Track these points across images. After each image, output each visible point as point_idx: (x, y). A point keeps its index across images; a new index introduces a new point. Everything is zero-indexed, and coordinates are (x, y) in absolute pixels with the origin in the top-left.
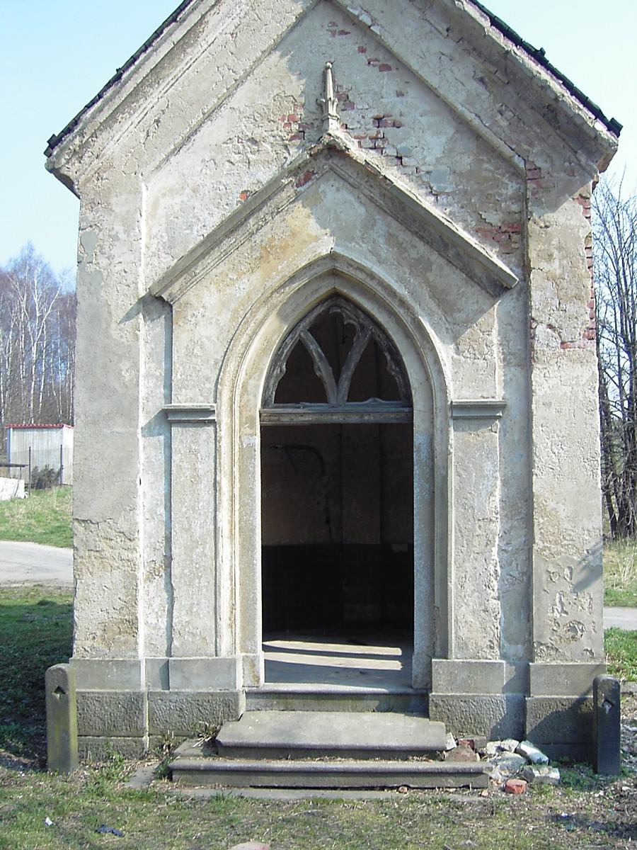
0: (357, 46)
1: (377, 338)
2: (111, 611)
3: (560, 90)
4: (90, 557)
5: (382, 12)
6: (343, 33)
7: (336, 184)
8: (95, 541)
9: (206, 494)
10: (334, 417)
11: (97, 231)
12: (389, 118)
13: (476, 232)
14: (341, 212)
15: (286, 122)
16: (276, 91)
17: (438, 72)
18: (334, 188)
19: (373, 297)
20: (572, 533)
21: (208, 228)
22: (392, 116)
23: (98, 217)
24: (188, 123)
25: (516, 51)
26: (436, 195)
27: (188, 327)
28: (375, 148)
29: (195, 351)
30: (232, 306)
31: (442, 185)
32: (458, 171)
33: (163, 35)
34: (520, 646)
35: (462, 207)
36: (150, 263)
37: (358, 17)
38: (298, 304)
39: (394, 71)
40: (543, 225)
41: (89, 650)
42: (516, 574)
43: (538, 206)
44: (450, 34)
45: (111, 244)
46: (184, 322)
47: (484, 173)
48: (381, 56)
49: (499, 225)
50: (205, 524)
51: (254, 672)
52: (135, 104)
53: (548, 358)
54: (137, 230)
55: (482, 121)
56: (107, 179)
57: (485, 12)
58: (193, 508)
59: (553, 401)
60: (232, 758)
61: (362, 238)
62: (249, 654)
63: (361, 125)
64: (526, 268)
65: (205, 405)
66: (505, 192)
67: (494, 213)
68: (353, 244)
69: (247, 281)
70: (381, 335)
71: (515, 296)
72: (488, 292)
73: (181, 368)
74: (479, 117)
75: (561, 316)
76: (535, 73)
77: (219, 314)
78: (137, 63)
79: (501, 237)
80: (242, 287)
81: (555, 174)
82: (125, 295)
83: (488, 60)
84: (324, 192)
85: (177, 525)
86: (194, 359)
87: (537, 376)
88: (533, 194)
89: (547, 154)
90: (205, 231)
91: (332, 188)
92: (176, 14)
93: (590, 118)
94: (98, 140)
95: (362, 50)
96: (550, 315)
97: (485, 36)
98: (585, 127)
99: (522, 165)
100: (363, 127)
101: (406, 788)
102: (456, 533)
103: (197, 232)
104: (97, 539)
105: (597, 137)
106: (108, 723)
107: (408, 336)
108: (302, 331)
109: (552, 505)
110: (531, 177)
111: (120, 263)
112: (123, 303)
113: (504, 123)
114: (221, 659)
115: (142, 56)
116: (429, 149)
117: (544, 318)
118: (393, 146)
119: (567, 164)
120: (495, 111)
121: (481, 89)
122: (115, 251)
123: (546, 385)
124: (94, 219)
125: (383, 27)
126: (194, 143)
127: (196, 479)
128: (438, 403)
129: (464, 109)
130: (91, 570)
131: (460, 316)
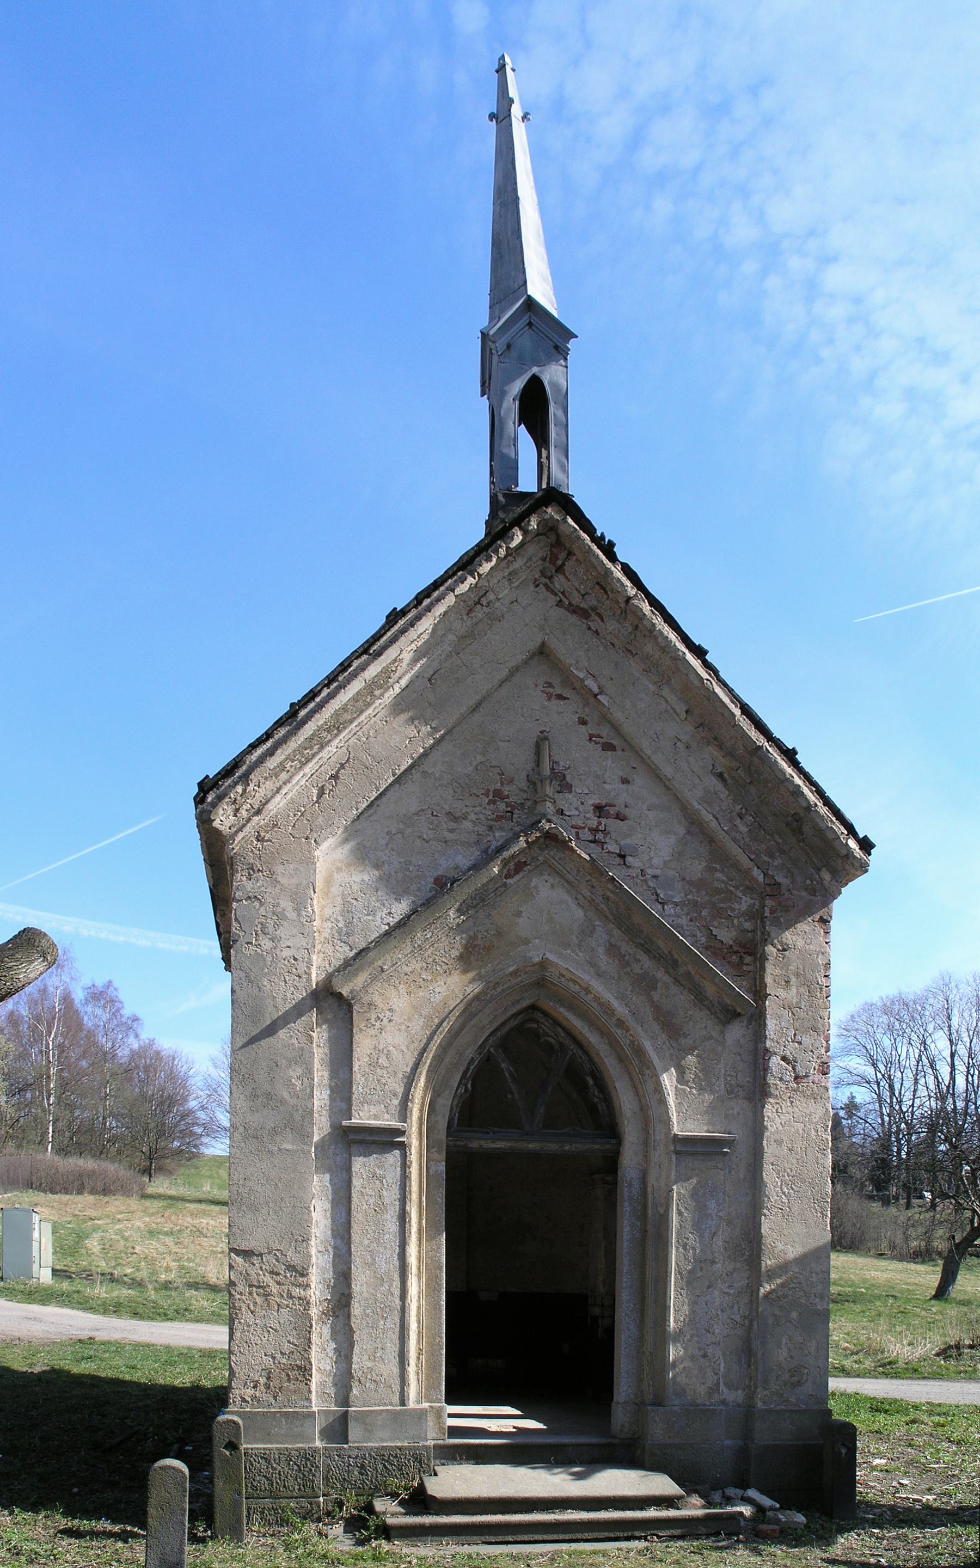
0: (578, 716)
1: (579, 1060)
2: (279, 1356)
3: (814, 798)
4: (250, 1293)
5: (611, 679)
6: (560, 697)
7: (551, 880)
8: (258, 1275)
9: (392, 1226)
10: (530, 1146)
11: (257, 904)
12: (612, 808)
13: (706, 948)
14: (556, 914)
15: (491, 797)
16: (479, 758)
17: (673, 761)
18: (548, 884)
19: (584, 1015)
20: (801, 1276)
21: (395, 916)
22: (615, 806)
23: (259, 887)
24: (375, 784)
25: (768, 747)
26: (663, 904)
27: (372, 1032)
28: (594, 841)
29: (380, 1061)
30: (425, 1012)
31: (670, 893)
32: (688, 879)
33: (351, 669)
34: (740, 1392)
35: (691, 920)
36: (323, 950)
37: (582, 680)
38: (496, 1015)
39: (619, 752)
41: (249, 1399)
42: (737, 1318)
43: (776, 926)
44: (689, 718)
45: (275, 923)
46: (366, 1026)
47: (717, 884)
48: (605, 731)
49: (731, 943)
50: (391, 1259)
51: (439, 1423)
52: (308, 751)
53: (781, 1093)
54: (310, 909)
55: (720, 824)
56: (270, 841)
57: (735, 698)
58: (377, 1240)
59: (785, 1138)
61: (579, 946)
62: (434, 1404)
63: (580, 812)
64: (760, 994)
65: (395, 1124)
66: (738, 907)
67: (726, 929)
69: (443, 984)
70: (583, 1057)
71: (745, 1022)
72: (718, 1018)
73: (363, 1079)
74: (717, 819)
75: (796, 1048)
76: (788, 776)
77: (409, 1020)
78: (318, 699)
79: (731, 956)
80: (437, 990)
82: (296, 987)
83: (730, 754)
84: (536, 887)
85: (357, 1260)
86: (378, 1070)
87: (769, 1110)
88: (772, 912)
89: (788, 868)
90: (391, 919)
91: (546, 884)
92: (368, 644)
93: (842, 833)
94: (260, 790)
95: (583, 722)
96: (785, 1046)
97: (735, 725)
98: (837, 843)
99: (761, 878)
100: (582, 815)
101: (655, 1537)
102: (676, 1274)
103: (382, 919)
104: (261, 1273)
105: (849, 853)
106: (277, 1483)
107: (621, 1059)
108: (492, 1046)
109: (780, 1246)
110: (770, 893)
112: (292, 996)
113: (744, 829)
114: (410, 1409)
115: (325, 692)
116: (656, 849)
117: (780, 1050)
118: (616, 841)
119: (808, 882)
120: (734, 814)
121: (720, 787)
123: (778, 1120)
125: (611, 698)
126: (378, 808)
127: (380, 1208)
129: (700, 807)
130: (252, 1308)
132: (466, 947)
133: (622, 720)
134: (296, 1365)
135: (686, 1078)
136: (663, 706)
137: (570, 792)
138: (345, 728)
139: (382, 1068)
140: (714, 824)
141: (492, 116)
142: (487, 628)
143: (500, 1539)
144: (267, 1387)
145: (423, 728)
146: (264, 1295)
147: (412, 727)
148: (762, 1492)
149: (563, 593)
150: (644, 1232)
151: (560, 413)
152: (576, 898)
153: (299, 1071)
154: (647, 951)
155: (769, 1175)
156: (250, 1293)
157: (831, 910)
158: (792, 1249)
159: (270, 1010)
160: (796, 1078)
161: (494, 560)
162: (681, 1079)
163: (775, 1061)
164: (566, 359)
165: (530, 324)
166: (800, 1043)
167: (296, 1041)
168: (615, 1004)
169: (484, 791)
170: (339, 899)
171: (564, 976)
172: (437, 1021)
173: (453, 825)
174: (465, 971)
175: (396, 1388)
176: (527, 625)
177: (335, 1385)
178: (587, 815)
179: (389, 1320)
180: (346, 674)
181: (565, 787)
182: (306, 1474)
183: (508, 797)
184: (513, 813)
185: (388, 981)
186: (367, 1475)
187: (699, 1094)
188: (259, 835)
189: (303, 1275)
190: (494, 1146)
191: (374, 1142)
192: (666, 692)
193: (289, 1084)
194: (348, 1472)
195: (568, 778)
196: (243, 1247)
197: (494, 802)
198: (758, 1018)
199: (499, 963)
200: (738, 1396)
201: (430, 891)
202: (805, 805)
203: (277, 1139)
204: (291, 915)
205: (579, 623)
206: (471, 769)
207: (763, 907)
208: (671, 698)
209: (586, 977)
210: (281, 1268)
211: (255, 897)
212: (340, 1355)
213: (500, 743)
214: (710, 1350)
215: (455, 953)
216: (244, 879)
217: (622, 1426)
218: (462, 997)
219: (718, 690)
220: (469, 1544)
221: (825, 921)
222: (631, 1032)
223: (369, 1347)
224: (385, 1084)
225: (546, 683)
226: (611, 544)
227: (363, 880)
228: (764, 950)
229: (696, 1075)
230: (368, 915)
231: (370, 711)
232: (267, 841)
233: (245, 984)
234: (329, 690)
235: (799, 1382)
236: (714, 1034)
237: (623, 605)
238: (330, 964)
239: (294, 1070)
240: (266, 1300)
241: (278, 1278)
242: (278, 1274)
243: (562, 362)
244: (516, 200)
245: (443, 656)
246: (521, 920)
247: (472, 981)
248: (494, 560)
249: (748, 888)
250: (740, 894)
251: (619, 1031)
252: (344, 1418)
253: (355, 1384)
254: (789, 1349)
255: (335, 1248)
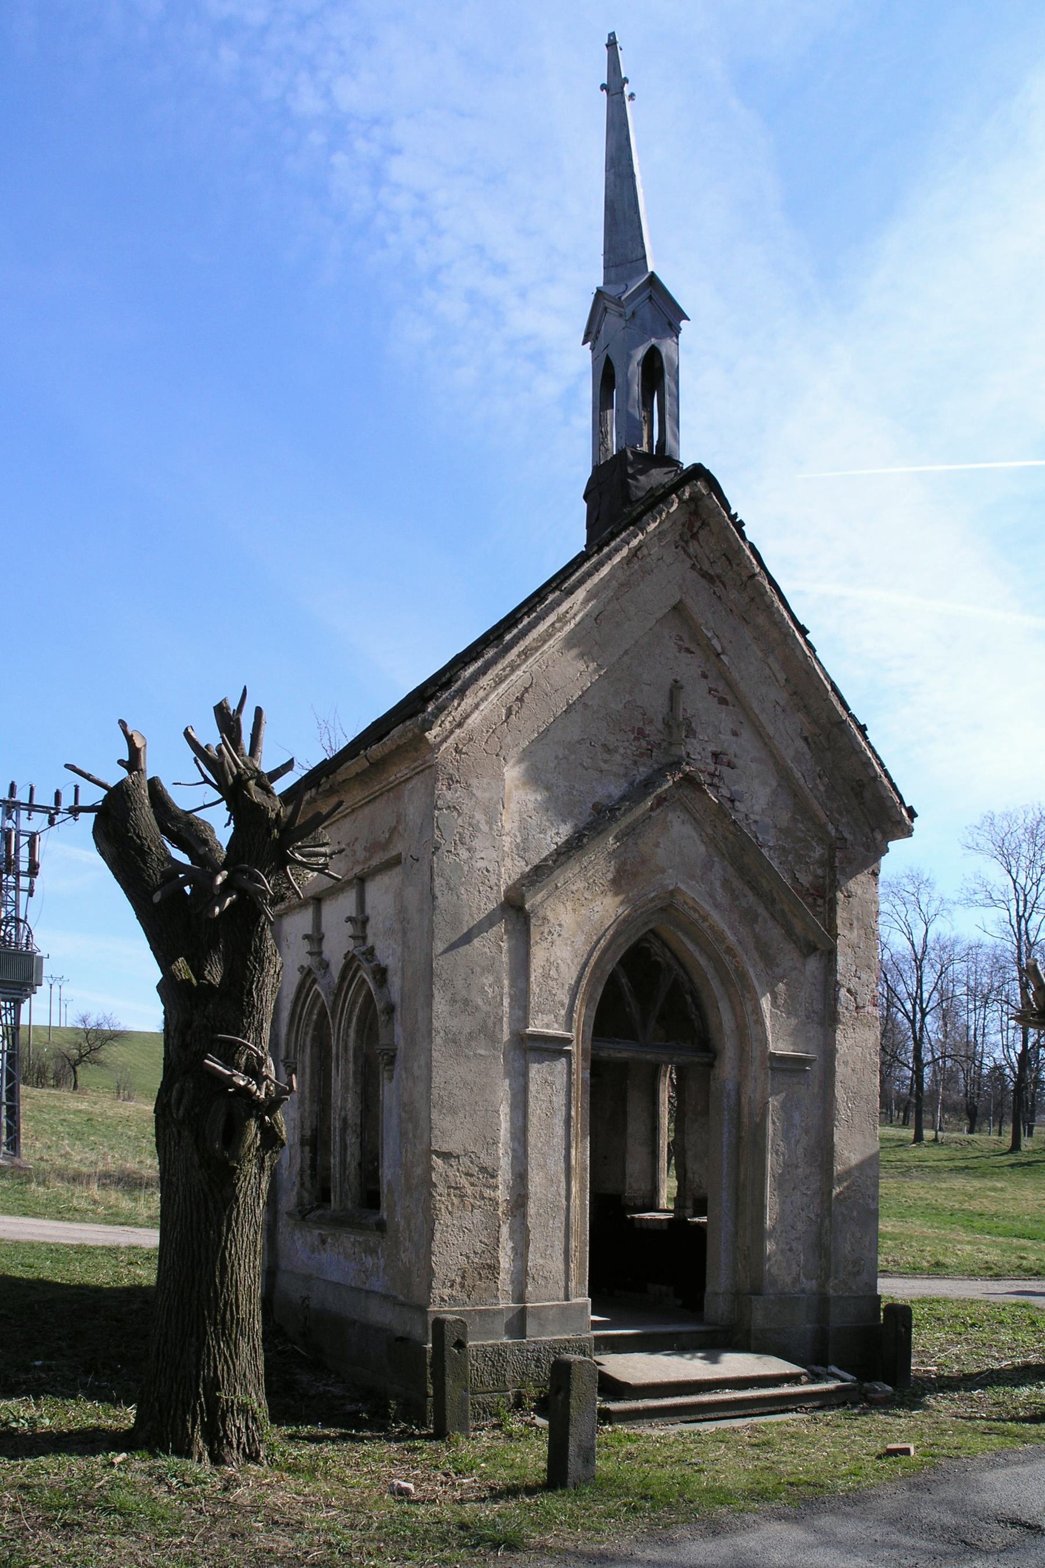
0: (701, 669)
2: (472, 1255)
4: (449, 1195)
6: (688, 651)
8: (455, 1176)
9: (560, 1130)
11: (455, 814)
16: (628, 697)
21: (562, 836)
22: (727, 755)
27: (545, 945)
29: (551, 972)
30: (586, 929)
34: (814, 1281)
37: (709, 639)
40: (846, 894)
41: (446, 1298)
42: (812, 1216)
46: (540, 939)
47: (799, 834)
48: (721, 686)
49: (808, 886)
54: (500, 824)
59: (850, 1061)
61: (702, 879)
68: (694, 882)
71: (818, 957)
73: (538, 989)
80: (596, 909)
81: (856, 847)
82: (488, 898)
84: (671, 822)
86: (550, 982)
95: (704, 676)
99: (833, 833)
109: (846, 1154)
111: (482, 858)
121: (806, 749)
122: (476, 843)
124: (452, 799)
127: (550, 1114)
128: (756, 1053)
130: (450, 1208)
131: (779, 971)
132: (618, 871)
133: (739, 679)
134: (487, 1264)
135: (779, 1003)
136: (768, 671)
137: (695, 738)
138: (532, 655)
139: (553, 979)
140: (802, 781)
141: (603, 87)
142: (640, 579)
143: (693, 1418)
144: (462, 1286)
145: (591, 664)
146: (461, 1196)
147: (582, 662)
148: (840, 1368)
149: (696, 557)
150: (739, 1139)
151: (673, 386)
152: (701, 835)
153: (491, 979)
154: (753, 888)
155: (839, 1093)
156: (449, 1195)
157: (879, 865)
158: (853, 1157)
159: (466, 919)
160: (857, 1008)
161: (658, 521)
162: (774, 1003)
163: (843, 992)
164: (677, 337)
165: (650, 298)
166: (859, 978)
167: (488, 951)
168: (728, 933)
169: (630, 728)
170: (517, 815)
171: (687, 904)
172: (595, 938)
173: (606, 756)
174: (616, 894)
175: (562, 1284)
176: (669, 582)
177: (512, 1282)
178: (707, 761)
179: (557, 1219)
180: (543, 606)
181: (691, 733)
182: (499, 1369)
183: (648, 736)
184: (652, 751)
185: (558, 897)
186: (542, 1368)
187: (788, 1018)
188: (457, 747)
189: (493, 1177)
190: (619, 1055)
191: (546, 1050)
192: (771, 660)
193: (482, 991)
194: (527, 1365)
195: (693, 725)
196: (444, 1150)
197: (636, 739)
198: (831, 954)
199: (643, 888)
200: (811, 1285)
201: (590, 816)
202: (873, 775)
203: (473, 1043)
204: (484, 827)
205: (707, 587)
206: (621, 706)
207: (834, 857)
208: (776, 667)
209: (707, 907)
210: (475, 1170)
211: (454, 807)
212: (517, 1254)
213: (643, 686)
214: (794, 1245)
215: (610, 876)
216: (444, 788)
217: (723, 1314)
218: (614, 917)
219: (817, 667)
220: (672, 1424)
221: (875, 874)
222: (737, 959)
223: (541, 1245)
224: (555, 995)
225: (678, 635)
226: (741, 523)
227: (536, 800)
228: (835, 895)
229: (785, 1001)
230: (540, 833)
231: (551, 642)
232: (464, 754)
233: (446, 892)
234: (529, 619)
235: (858, 1271)
236: (797, 965)
237: (744, 579)
238: (509, 877)
239: (486, 978)
240: (462, 1200)
241: (472, 1180)
242: (472, 1175)
243: (674, 338)
244: (632, 176)
245: (606, 600)
246: (659, 850)
247: (622, 903)
248: (658, 521)
249: (820, 839)
250: (814, 844)
251: (727, 957)
252: (522, 1313)
253: (530, 1281)
254: (852, 1243)
255: (513, 1150)
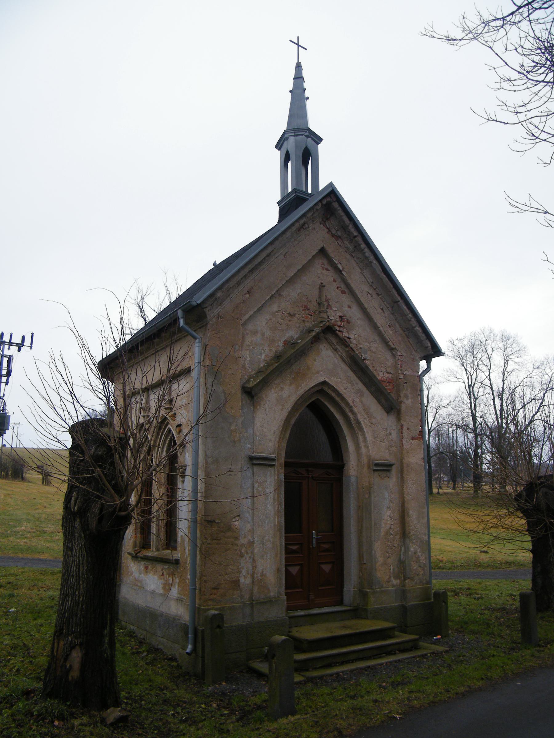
6: (327, 269)
48: (343, 286)
60: (262, 461)
95: (335, 281)
137: (331, 309)
173: (290, 318)
